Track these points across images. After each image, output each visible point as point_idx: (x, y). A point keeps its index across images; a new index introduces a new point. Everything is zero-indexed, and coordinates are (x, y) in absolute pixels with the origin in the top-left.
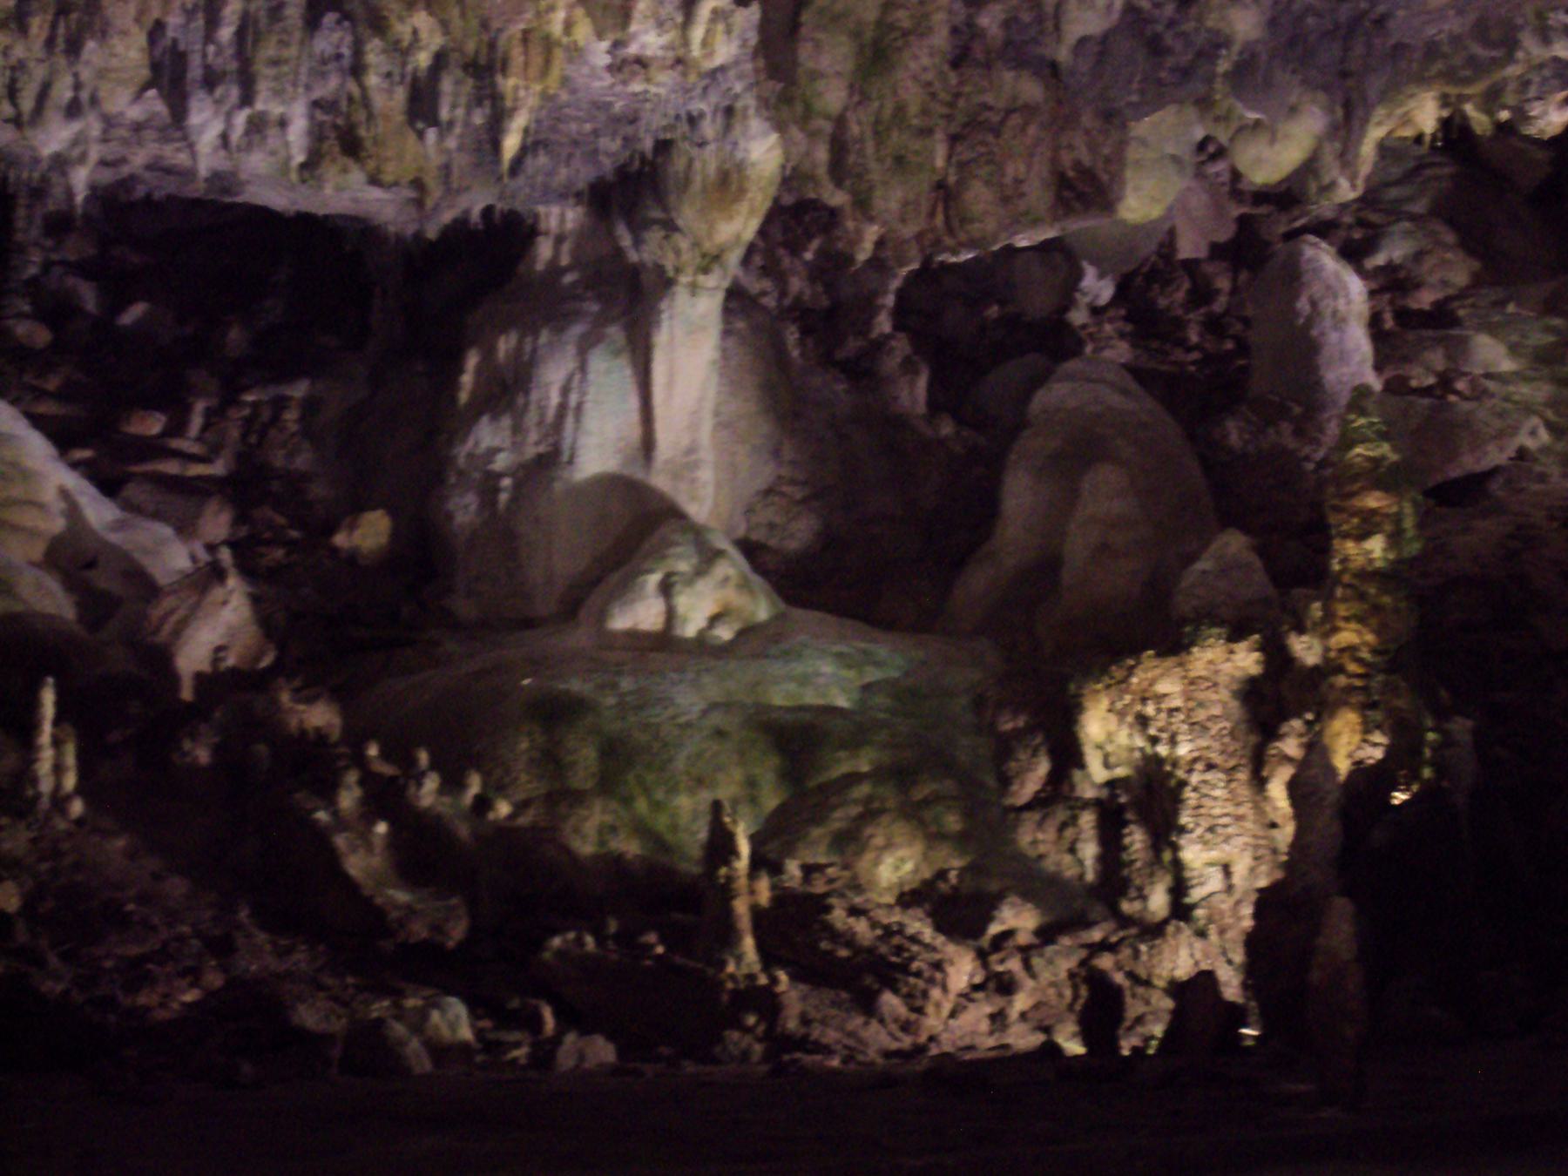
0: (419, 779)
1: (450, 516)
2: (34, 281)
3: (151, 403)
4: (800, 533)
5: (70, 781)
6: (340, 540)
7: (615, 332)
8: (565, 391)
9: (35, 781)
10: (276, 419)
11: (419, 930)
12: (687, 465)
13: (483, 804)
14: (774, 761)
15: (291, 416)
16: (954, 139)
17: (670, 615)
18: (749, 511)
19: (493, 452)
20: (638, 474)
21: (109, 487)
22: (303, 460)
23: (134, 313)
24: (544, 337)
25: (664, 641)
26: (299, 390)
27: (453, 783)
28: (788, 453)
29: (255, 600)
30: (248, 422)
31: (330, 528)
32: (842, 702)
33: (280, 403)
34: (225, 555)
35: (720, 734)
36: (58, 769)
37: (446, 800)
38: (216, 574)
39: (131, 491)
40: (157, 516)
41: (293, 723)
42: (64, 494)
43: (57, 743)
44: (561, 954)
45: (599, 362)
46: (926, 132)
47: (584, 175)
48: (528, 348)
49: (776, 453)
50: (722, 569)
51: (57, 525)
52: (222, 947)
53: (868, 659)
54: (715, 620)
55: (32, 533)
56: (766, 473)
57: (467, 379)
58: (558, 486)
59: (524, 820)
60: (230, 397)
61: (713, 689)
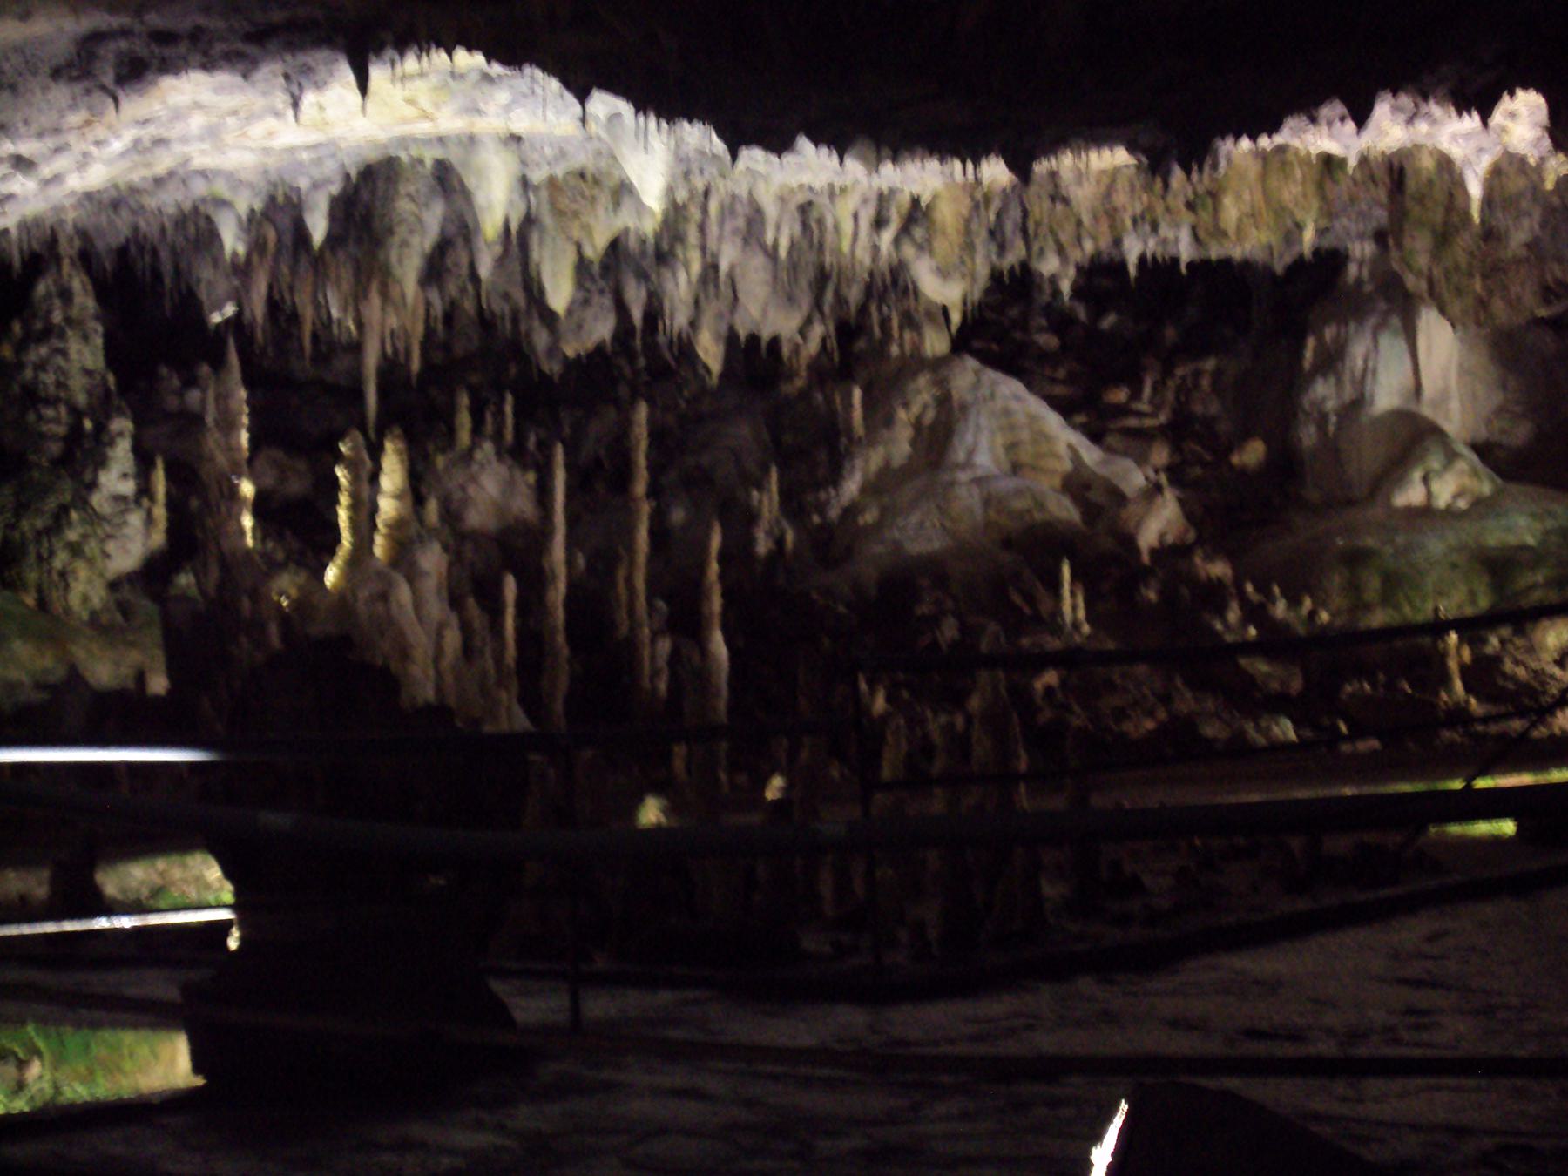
0: (1273, 602)
1: (1300, 440)
2: (1049, 305)
3: (1117, 380)
4: (1520, 434)
5: (1081, 614)
6: (1236, 459)
7: (1395, 321)
8: (1366, 361)
9: (1062, 615)
10: (1196, 385)
11: (1275, 686)
12: (1444, 396)
13: (1313, 614)
14: (1486, 579)
15: (1205, 383)
16: (1484, 277)
17: (1429, 494)
18: (1489, 422)
19: (1324, 400)
20: (1412, 407)
21: (1096, 437)
22: (1214, 408)
23: (1108, 321)
24: (1352, 326)
25: (1426, 513)
26: (1210, 364)
27: (1294, 601)
28: (1512, 383)
29: (1182, 502)
30: (1178, 390)
31: (1229, 450)
32: (1530, 541)
33: (1197, 374)
34: (1163, 479)
35: (1454, 566)
36: (1074, 608)
37: (1292, 614)
38: (1157, 489)
39: (1112, 440)
40: (1126, 454)
41: (1202, 574)
42: (1070, 447)
43: (1073, 593)
44: (1352, 695)
45: (1385, 340)
46: (1471, 275)
47: (1372, 226)
48: (1342, 334)
49: (1504, 387)
50: (1461, 465)
51: (1067, 466)
52: (1166, 699)
53: (1551, 514)
54: (1456, 496)
55: (1054, 472)
56: (1497, 398)
57: (1308, 354)
58: (1364, 419)
59: (1338, 622)
60: (1167, 372)
61: (1452, 538)
